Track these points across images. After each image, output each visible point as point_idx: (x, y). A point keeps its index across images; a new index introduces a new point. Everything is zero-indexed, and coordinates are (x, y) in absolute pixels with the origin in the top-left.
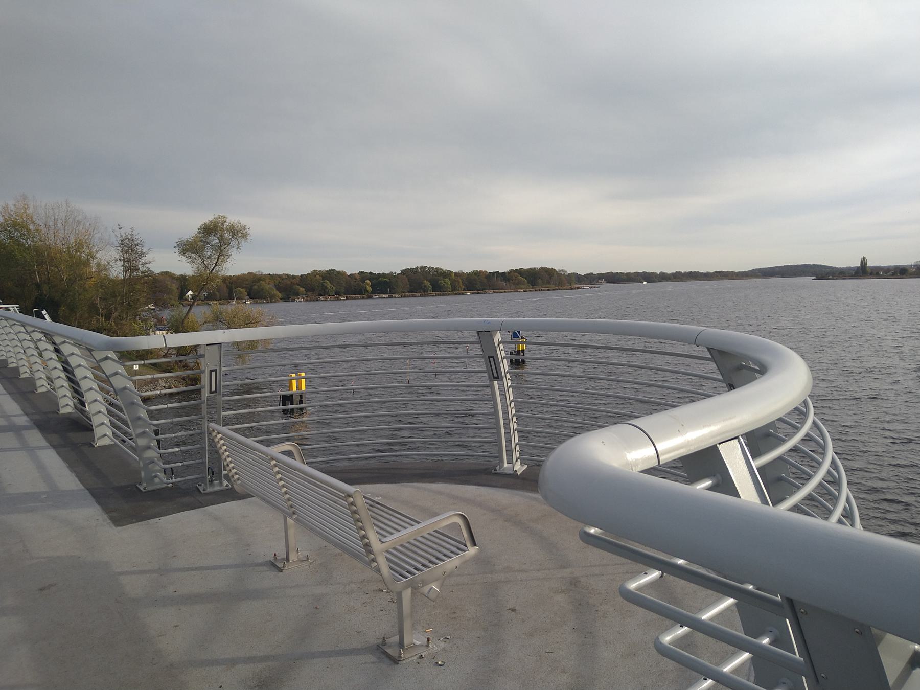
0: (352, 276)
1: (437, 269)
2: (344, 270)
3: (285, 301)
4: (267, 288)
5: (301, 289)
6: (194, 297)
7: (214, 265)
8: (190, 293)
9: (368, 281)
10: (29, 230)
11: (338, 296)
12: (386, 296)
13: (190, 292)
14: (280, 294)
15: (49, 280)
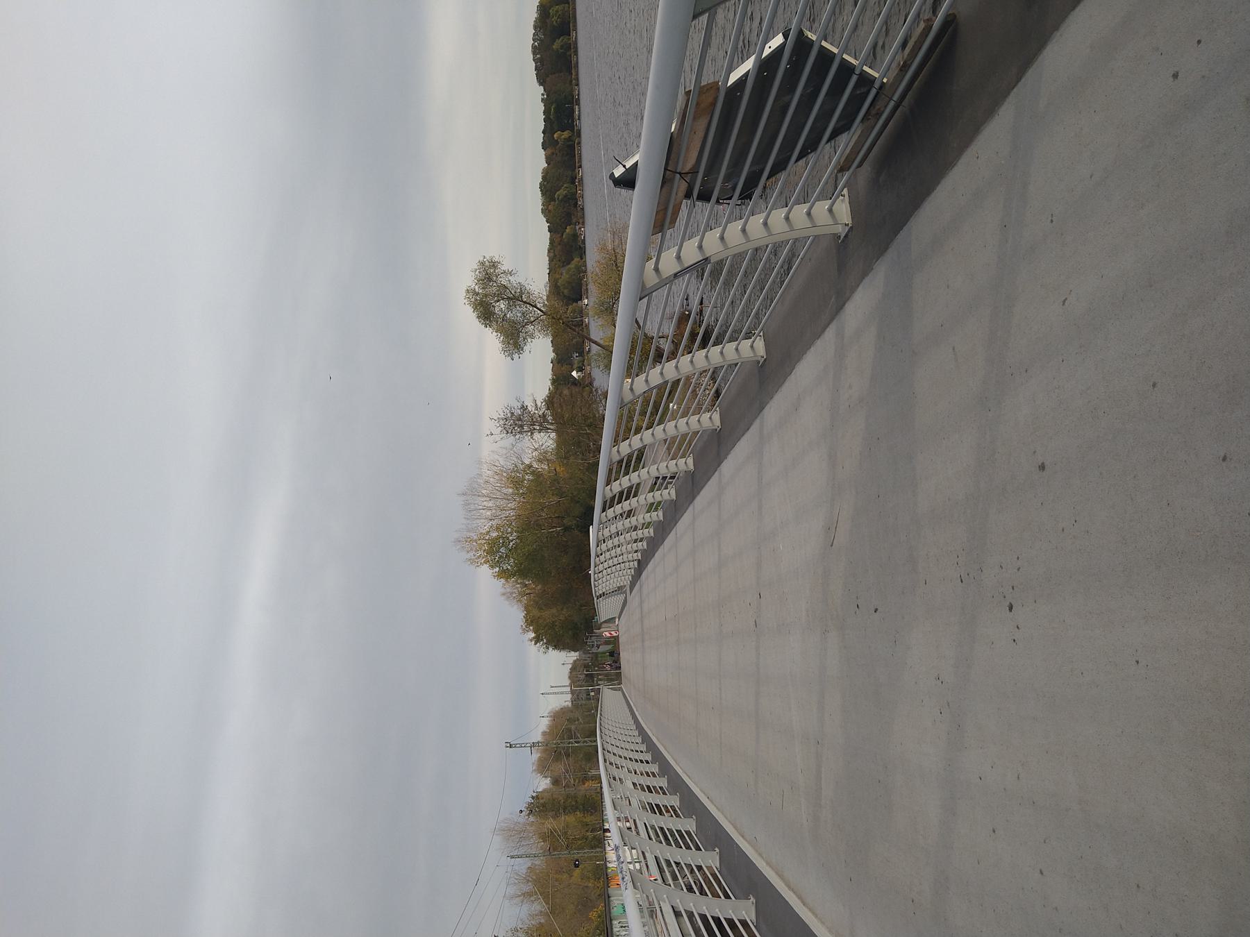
0: (549, 160)
1: (535, 28)
2: (541, 171)
3: (585, 252)
4: (567, 276)
5: (567, 231)
6: (580, 369)
7: (535, 309)
8: (574, 374)
9: (555, 136)
10: (498, 538)
11: (577, 180)
12: (577, 109)
13: (572, 374)
14: (575, 259)
15: (559, 517)
